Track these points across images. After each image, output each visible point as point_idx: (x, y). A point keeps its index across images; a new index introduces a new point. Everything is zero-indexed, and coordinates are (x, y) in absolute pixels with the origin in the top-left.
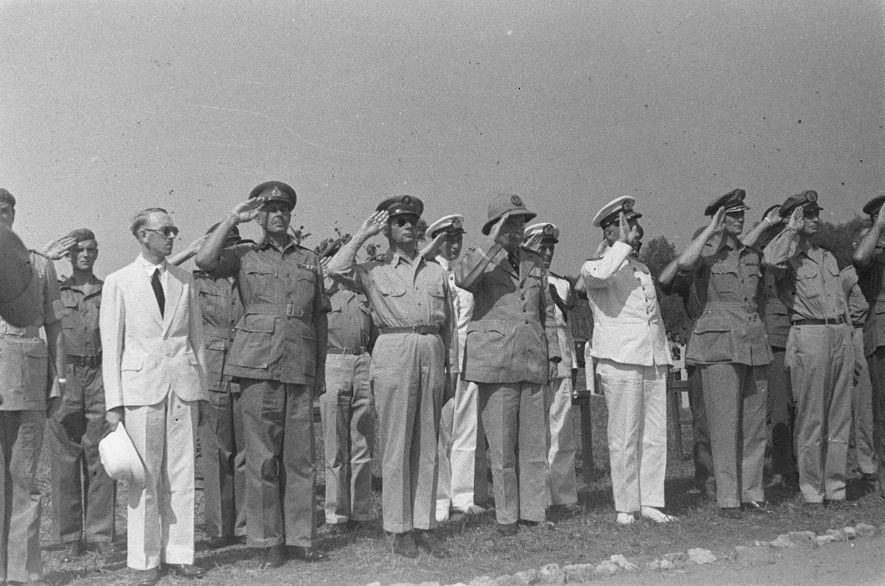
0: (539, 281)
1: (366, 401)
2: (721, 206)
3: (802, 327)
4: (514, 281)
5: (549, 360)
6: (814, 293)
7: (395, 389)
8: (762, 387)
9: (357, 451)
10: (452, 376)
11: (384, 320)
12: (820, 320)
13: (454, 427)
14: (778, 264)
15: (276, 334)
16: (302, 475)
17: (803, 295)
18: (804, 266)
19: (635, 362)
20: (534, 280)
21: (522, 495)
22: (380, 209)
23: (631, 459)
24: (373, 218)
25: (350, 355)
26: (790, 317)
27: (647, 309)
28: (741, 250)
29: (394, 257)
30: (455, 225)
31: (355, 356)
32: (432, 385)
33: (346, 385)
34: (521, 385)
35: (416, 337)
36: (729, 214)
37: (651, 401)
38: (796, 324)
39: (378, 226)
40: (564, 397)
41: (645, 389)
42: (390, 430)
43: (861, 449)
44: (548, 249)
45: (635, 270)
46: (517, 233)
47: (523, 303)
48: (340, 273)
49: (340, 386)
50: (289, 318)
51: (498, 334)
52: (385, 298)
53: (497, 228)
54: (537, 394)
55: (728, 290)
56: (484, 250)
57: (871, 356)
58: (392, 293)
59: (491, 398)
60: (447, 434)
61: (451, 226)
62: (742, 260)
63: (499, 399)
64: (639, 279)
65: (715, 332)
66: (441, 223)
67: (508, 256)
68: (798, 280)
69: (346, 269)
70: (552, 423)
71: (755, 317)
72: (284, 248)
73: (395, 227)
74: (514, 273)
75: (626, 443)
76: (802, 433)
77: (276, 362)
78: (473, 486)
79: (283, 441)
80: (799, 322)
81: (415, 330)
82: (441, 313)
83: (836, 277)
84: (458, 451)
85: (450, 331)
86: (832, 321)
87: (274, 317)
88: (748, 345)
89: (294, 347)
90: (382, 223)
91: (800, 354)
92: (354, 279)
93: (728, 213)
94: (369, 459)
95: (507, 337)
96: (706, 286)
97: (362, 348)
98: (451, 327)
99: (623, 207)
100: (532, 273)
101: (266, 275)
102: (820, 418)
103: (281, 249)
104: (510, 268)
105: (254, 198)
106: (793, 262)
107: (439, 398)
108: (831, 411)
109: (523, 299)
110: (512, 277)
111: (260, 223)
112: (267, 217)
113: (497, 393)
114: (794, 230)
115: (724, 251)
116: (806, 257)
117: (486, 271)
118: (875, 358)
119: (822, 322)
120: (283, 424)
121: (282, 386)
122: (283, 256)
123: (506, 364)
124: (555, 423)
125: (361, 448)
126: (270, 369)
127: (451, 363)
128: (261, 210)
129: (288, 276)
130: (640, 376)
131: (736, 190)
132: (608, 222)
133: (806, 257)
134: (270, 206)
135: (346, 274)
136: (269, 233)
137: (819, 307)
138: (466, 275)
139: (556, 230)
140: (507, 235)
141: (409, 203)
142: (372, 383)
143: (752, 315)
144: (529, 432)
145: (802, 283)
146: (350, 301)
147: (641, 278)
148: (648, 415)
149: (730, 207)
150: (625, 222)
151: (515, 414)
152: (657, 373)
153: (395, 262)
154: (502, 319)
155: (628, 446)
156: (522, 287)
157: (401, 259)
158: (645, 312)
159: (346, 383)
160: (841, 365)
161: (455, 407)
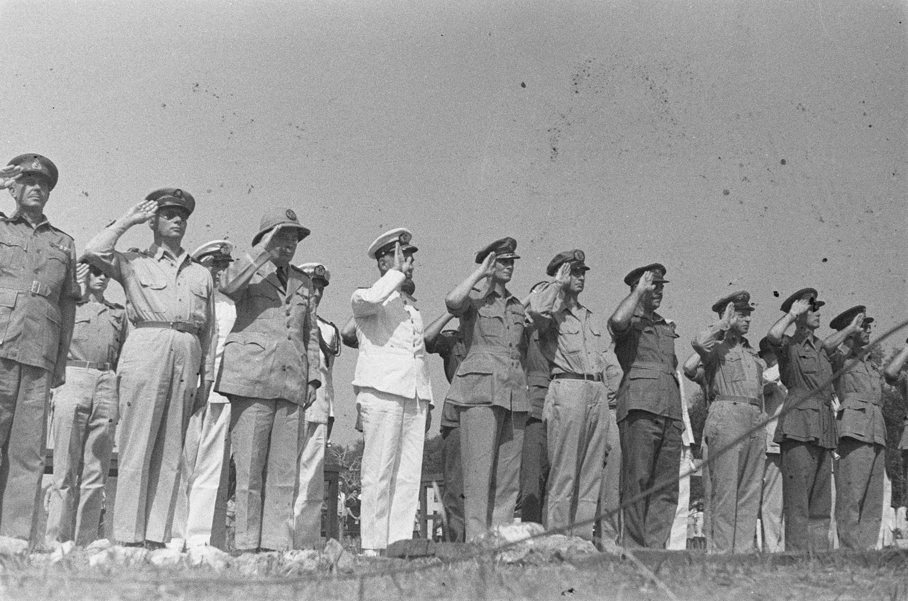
0: (306, 301)
1: (105, 421)
2: (492, 251)
3: (562, 381)
4: (280, 295)
5: (308, 383)
6: (575, 348)
7: (143, 385)
8: (519, 435)
9: (89, 475)
10: (206, 383)
11: (140, 313)
12: (579, 374)
13: (197, 462)
14: (543, 313)
15: (17, 309)
16: (26, 466)
17: (564, 349)
18: (567, 322)
19: (398, 393)
20: (301, 298)
21: (266, 520)
22: (149, 198)
23: (383, 494)
24: (141, 206)
25: (93, 370)
26: (551, 371)
27: (415, 341)
28: (507, 299)
29: (158, 251)
30: (222, 250)
31: (99, 371)
32: (184, 386)
33: (85, 400)
34: (277, 403)
35: (172, 333)
36: (500, 260)
37: (408, 435)
38: (556, 378)
39: (145, 214)
40: (317, 444)
41: (404, 422)
42: (132, 431)
43: (606, 531)
44: (317, 290)
45: (405, 303)
46: (288, 247)
47: (288, 318)
48: (99, 254)
49: (78, 401)
50: (34, 295)
51: (257, 346)
52: (144, 290)
53: (268, 237)
54: (293, 415)
55: (493, 334)
56: (253, 257)
57: (623, 421)
58: (151, 285)
59: (243, 413)
60: (189, 469)
61: (219, 251)
62: (508, 308)
63: (252, 415)
64: (408, 312)
65: (476, 374)
66: (208, 247)
67: (276, 271)
68: (561, 335)
69: (106, 252)
70: (303, 471)
71: (518, 364)
72: (37, 224)
73: (163, 219)
74: (281, 288)
75: (380, 475)
76: (554, 488)
77: (13, 340)
78: (210, 526)
79: (11, 427)
80: (559, 376)
81: (172, 326)
82: (201, 313)
83: (597, 337)
84: (200, 489)
85: (209, 336)
86: (590, 377)
87: (17, 292)
88: (508, 390)
89: (36, 326)
90: (149, 213)
91: (558, 407)
92: (113, 263)
93: (500, 259)
94: (101, 485)
95: (267, 352)
96: (472, 326)
97: (108, 364)
98: (211, 332)
99: (399, 238)
100: (300, 291)
101: (14, 247)
102: (572, 472)
103: (34, 225)
104: (278, 283)
105: (12, 166)
106: (557, 318)
107: (190, 402)
108: (583, 466)
109: (288, 315)
110: (278, 292)
111: (15, 196)
112: (24, 189)
113: (251, 409)
114: (560, 283)
115: (491, 297)
116: (570, 313)
117: (251, 282)
118: (626, 423)
119: (581, 377)
120: (13, 410)
121: (16, 368)
122: (35, 232)
123: (264, 378)
124: (305, 470)
125: (93, 472)
126: (5, 346)
127: (207, 370)
128: (18, 180)
129: (38, 251)
130: (401, 408)
131: (507, 238)
132: (382, 253)
133: (570, 313)
134: (28, 177)
135: (104, 257)
136: (23, 207)
137: (579, 362)
138: (231, 280)
139: (328, 272)
140: (278, 248)
141: (180, 197)
142: (119, 378)
143: (515, 361)
144: (281, 453)
145: (565, 338)
146: (101, 313)
147: (410, 311)
148: (407, 442)
149: (501, 254)
150: (401, 251)
151: (267, 433)
152: (418, 407)
153: (158, 256)
154: (264, 333)
155: (382, 479)
156: (288, 303)
157: (165, 253)
158: (412, 344)
159: (87, 399)
160: (596, 422)
161: (201, 440)
